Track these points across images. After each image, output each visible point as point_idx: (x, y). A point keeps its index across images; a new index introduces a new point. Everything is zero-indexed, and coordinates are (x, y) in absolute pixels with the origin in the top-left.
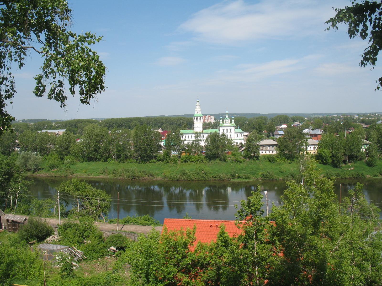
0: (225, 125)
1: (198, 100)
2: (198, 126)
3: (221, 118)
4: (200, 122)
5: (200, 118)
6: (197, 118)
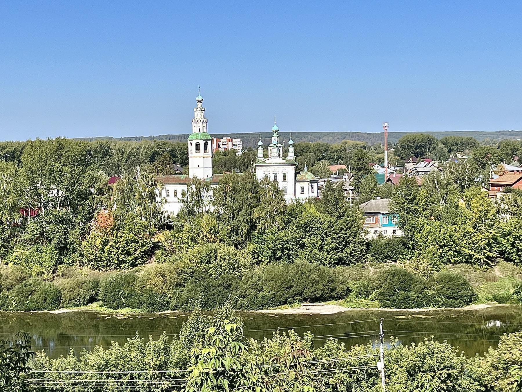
1: (199, 98)
2: (200, 166)
3: (260, 143)
4: (206, 155)
5: (206, 144)
6: (198, 146)
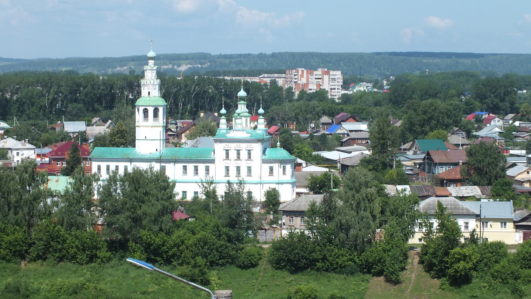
0: (232, 134)
4: (156, 124)
6: (146, 111)
